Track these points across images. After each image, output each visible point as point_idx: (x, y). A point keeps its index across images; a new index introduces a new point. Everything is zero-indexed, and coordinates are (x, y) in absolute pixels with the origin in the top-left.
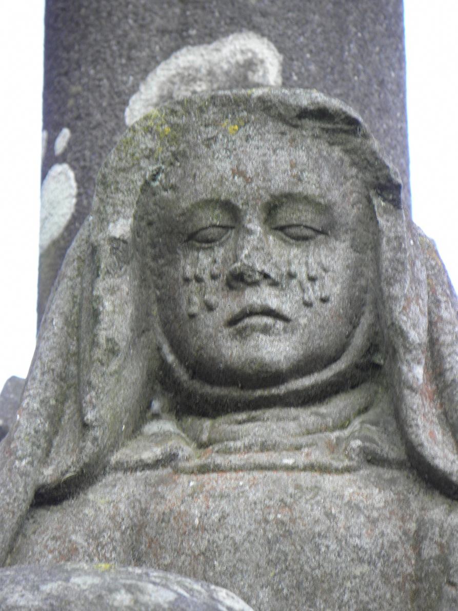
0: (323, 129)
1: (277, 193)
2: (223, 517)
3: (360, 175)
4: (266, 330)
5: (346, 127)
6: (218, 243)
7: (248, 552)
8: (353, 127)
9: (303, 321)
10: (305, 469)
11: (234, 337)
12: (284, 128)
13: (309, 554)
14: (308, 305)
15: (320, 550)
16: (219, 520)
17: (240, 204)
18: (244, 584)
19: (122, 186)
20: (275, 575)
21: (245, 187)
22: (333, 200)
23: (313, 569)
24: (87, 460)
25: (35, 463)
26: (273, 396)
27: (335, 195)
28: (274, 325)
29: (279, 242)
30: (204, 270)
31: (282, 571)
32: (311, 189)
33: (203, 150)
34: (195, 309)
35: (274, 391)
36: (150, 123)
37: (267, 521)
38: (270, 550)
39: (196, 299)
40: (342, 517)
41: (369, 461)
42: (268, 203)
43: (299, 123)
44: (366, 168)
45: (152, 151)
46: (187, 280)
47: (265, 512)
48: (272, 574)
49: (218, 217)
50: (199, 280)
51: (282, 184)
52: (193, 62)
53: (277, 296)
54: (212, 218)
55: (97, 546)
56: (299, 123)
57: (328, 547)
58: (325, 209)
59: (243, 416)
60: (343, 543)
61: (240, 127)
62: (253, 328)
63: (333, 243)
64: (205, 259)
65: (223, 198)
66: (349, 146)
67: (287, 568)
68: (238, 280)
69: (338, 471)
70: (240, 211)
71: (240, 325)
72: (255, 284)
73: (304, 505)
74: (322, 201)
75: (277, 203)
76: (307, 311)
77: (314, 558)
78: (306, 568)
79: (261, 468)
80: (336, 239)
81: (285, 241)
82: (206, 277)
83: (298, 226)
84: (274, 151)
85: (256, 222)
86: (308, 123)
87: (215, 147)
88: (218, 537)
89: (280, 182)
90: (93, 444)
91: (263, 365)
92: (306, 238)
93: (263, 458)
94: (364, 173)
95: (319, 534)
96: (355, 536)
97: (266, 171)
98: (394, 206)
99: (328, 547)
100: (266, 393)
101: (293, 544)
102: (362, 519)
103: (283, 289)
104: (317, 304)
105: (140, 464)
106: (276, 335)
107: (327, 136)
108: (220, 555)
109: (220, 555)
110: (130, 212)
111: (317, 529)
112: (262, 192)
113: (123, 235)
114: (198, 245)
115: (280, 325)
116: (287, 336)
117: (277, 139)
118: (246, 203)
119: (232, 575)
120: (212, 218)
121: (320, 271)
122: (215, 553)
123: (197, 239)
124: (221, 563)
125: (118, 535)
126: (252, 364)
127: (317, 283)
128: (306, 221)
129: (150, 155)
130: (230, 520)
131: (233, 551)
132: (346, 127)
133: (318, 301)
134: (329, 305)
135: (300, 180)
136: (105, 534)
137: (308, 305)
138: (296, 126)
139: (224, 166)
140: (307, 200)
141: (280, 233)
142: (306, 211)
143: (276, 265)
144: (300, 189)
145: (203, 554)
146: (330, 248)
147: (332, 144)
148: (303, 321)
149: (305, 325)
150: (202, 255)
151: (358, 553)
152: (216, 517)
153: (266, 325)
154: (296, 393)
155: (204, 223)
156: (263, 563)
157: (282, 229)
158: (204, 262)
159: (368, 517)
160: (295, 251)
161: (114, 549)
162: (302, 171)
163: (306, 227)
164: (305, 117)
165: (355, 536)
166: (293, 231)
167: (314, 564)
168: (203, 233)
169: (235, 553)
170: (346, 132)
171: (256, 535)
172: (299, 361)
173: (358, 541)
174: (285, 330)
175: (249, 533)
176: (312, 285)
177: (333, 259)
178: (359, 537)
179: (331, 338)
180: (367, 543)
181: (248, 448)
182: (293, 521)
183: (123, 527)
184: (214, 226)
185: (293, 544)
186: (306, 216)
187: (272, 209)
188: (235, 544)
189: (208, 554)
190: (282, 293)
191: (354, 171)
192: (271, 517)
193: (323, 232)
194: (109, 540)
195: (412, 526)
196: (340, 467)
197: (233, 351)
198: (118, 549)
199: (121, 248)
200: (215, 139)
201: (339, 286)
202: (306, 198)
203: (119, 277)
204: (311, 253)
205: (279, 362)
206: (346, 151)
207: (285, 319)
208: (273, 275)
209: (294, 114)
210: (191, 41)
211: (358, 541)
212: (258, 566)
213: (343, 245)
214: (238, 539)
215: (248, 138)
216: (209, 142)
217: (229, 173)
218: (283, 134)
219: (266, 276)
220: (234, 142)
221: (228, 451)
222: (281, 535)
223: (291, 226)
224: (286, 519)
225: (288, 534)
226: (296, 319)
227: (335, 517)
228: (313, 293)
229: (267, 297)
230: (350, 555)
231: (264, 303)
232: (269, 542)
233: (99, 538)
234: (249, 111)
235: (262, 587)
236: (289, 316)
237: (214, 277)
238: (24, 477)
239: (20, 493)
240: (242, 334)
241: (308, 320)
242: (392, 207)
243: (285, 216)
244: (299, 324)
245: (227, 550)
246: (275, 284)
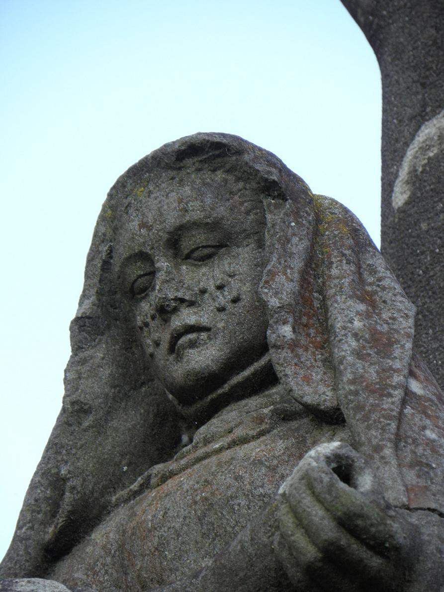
0: (201, 161)
1: (172, 229)
3: (248, 186)
4: (193, 344)
5: (217, 152)
6: (150, 289)
7: (187, 534)
8: (221, 151)
9: (220, 325)
10: (229, 447)
12: (171, 173)
13: (227, 517)
14: (221, 309)
15: (234, 509)
16: (163, 517)
17: (148, 250)
18: (191, 561)
20: (210, 544)
21: (148, 234)
22: (220, 216)
23: (234, 528)
24: (69, 508)
25: (36, 526)
26: (224, 394)
27: (222, 211)
28: (198, 338)
29: (191, 268)
30: (146, 315)
31: (214, 539)
32: (196, 215)
35: (220, 391)
37: (195, 503)
38: (202, 524)
40: (247, 475)
41: (284, 419)
42: (168, 240)
43: (182, 165)
44: (249, 178)
47: (194, 496)
48: (207, 545)
49: (140, 268)
51: (173, 220)
52: (429, 134)
53: (195, 313)
54: (135, 271)
55: (94, 574)
56: (182, 165)
57: (239, 505)
58: (214, 226)
60: (250, 496)
61: (144, 187)
63: (235, 251)
65: (137, 251)
66: (228, 167)
67: (216, 536)
68: (164, 312)
69: (254, 438)
70: (150, 255)
72: (175, 310)
74: (208, 220)
75: (176, 237)
76: (223, 316)
77: (232, 518)
78: (229, 529)
79: (199, 460)
80: (238, 247)
81: (195, 265)
83: (197, 249)
84: (167, 196)
85: (163, 259)
86: (188, 162)
88: (163, 532)
89: (172, 220)
90: (71, 493)
91: (197, 374)
92: (209, 257)
94: (249, 184)
95: (231, 497)
96: (259, 486)
97: (161, 215)
98: (283, 199)
99: (239, 505)
100: (214, 395)
101: (216, 514)
102: (264, 470)
103: (200, 305)
104: (229, 306)
105: (131, 493)
106: (203, 345)
107: (206, 166)
108: (168, 544)
109: (168, 544)
111: (229, 493)
112: (161, 234)
113: (84, 313)
114: (139, 296)
115: (204, 335)
116: (212, 342)
117: (169, 185)
118: (152, 248)
119: (180, 557)
121: (226, 278)
122: (164, 544)
124: (170, 551)
125: (109, 559)
126: (189, 377)
127: (226, 289)
128: (202, 242)
131: (176, 538)
132: (217, 152)
133: (230, 304)
134: (240, 304)
135: (186, 211)
136: (98, 563)
137: (221, 309)
138: (180, 169)
140: (195, 225)
141: (190, 261)
142: (199, 233)
143: (189, 288)
144: (188, 218)
145: (157, 549)
146: (234, 256)
147: (214, 171)
148: (220, 325)
149: (224, 327)
151: (263, 500)
153: (190, 340)
154: (239, 385)
155: (133, 277)
156: (199, 539)
157: (188, 257)
159: (268, 467)
160: (204, 270)
161: (106, 572)
162: (187, 203)
163: (203, 247)
164: (184, 158)
165: (259, 486)
166: (196, 254)
167: (233, 523)
168: (136, 285)
169: (178, 539)
170: (219, 156)
171: (190, 518)
172: (229, 359)
173: (261, 490)
174: (209, 338)
175: (185, 518)
176: (221, 293)
177: (237, 264)
178: (262, 487)
179: (255, 329)
180: (269, 490)
182: (213, 494)
183: (113, 552)
184: (140, 276)
185: (216, 514)
186: (198, 238)
187: (173, 241)
188: (176, 531)
189: (160, 548)
190: (199, 309)
191: (241, 185)
192: (199, 497)
193: (221, 246)
194: (102, 567)
196: (255, 434)
198: (110, 571)
199: (87, 324)
201: (248, 284)
202: (194, 223)
203: (93, 347)
204: (216, 266)
205: (208, 366)
206: (228, 171)
207: (207, 329)
208: (187, 298)
209: (173, 159)
210: (427, 118)
211: (261, 490)
212: (197, 542)
213: (247, 249)
214: (177, 526)
215: (150, 192)
218: (173, 178)
219: (182, 301)
220: (141, 201)
222: (207, 510)
223: (193, 251)
224: (208, 495)
226: (215, 326)
227: (241, 477)
228: (223, 299)
229: (188, 317)
230: (257, 504)
231: (183, 323)
232: (200, 520)
233: (94, 568)
234: (149, 171)
235: (203, 558)
236: (208, 325)
238: (24, 542)
239: (22, 556)
241: (225, 322)
242: (281, 201)
243: (187, 244)
244: (219, 329)
245: (172, 538)
246: (191, 304)
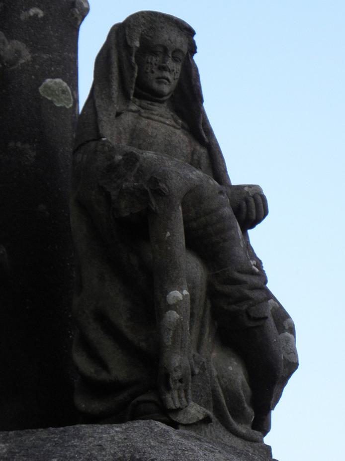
2: (157, 135)
4: (165, 84)
11: (156, 82)
17: (168, 48)
19: (136, 30)
33: (160, 29)
34: (148, 71)
36: (144, 15)
39: (149, 69)
45: (144, 24)
46: (148, 63)
50: (151, 64)
59: (149, 102)
62: (163, 82)
64: (154, 59)
71: (160, 80)
73: (173, 138)
82: (153, 63)
86: (185, 31)
87: (164, 30)
92: (177, 61)
93: (162, 119)
110: (138, 39)
115: (168, 83)
120: (161, 49)
123: (154, 53)
129: (144, 24)
130: (158, 136)
139: (166, 36)
150: (153, 57)
152: (155, 134)
158: (154, 60)
160: (175, 64)
181: (157, 115)
195: (192, 149)
197: (155, 85)
200: (163, 27)
215: (171, 30)
216: (162, 28)
217: (167, 39)
221: (152, 114)
223: (176, 57)
225: (170, 144)
237: (156, 65)
240: (160, 83)
246: (170, 72)
